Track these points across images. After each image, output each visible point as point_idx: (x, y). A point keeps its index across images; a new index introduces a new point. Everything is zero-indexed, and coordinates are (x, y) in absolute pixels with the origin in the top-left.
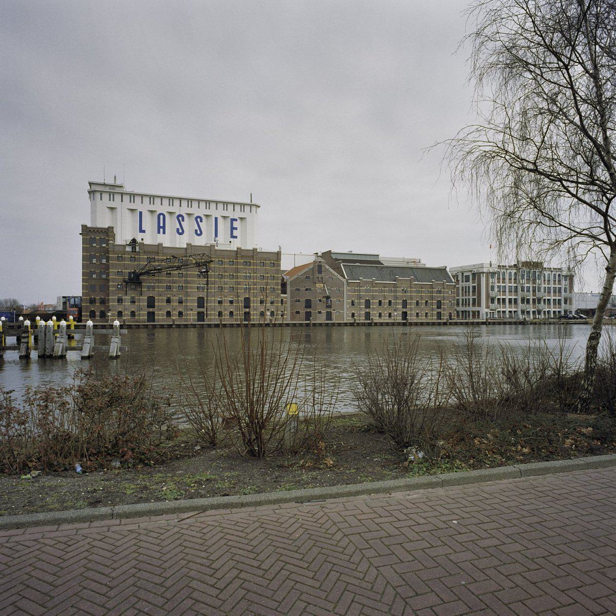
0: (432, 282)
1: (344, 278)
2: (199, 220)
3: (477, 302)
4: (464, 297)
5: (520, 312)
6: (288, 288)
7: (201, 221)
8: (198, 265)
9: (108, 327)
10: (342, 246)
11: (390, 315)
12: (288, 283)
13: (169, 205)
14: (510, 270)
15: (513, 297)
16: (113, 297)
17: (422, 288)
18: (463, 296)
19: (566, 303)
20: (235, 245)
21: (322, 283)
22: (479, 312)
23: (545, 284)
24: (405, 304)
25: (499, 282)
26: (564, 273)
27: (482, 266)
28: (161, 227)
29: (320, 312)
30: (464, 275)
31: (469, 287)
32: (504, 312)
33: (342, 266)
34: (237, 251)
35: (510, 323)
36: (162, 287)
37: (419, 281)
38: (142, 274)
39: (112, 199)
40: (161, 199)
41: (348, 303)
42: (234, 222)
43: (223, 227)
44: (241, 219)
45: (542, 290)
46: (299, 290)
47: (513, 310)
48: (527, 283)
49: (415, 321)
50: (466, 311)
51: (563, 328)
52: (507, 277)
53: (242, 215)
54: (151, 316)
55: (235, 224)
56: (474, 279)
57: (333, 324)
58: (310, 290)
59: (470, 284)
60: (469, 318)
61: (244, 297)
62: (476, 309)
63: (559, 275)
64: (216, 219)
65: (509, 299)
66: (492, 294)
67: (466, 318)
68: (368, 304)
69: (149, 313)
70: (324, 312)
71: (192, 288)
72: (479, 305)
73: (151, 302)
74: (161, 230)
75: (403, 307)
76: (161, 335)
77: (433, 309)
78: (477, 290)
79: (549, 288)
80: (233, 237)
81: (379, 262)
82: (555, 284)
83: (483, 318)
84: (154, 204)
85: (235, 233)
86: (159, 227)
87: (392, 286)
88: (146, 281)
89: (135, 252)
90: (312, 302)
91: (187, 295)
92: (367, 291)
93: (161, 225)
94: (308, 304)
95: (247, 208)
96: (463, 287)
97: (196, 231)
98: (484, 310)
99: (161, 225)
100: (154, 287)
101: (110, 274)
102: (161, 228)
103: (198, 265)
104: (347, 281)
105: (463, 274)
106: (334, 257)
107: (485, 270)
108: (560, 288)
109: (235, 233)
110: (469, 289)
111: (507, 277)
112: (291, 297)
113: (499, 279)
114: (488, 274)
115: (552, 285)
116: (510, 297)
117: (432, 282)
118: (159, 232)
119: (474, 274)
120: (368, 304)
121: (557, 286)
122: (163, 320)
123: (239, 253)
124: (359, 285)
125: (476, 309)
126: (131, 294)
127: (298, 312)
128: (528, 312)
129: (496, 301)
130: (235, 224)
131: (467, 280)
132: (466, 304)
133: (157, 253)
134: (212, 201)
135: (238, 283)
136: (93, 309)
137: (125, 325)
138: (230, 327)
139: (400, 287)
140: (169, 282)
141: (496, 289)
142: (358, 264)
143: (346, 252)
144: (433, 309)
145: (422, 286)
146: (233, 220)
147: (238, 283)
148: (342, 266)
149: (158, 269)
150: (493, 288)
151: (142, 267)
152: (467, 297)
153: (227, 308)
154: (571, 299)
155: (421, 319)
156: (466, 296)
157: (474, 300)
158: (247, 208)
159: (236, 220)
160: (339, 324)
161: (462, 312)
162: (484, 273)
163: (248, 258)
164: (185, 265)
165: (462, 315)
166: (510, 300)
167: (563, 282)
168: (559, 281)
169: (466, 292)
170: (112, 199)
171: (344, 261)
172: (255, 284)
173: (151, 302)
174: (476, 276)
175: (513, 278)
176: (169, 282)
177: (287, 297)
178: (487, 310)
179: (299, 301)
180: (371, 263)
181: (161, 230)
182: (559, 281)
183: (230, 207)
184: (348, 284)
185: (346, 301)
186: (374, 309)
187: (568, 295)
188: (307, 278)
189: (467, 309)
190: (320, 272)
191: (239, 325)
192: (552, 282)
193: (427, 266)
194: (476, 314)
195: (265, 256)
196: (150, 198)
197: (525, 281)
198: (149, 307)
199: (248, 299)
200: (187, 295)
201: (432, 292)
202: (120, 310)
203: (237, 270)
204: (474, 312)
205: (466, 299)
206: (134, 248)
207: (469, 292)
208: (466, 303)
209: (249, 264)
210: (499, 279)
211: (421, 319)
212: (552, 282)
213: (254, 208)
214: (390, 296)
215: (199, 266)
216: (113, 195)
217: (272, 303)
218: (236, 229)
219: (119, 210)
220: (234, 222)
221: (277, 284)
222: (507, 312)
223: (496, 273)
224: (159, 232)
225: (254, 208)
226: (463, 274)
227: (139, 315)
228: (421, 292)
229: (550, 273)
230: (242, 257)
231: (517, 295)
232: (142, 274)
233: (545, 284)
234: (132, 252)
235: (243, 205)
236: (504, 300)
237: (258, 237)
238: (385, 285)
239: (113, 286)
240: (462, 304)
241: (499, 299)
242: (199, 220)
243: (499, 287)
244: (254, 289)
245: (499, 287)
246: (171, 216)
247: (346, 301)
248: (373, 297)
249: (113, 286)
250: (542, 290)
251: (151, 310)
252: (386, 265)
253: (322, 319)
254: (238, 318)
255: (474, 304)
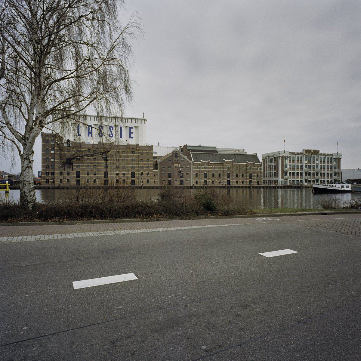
0: (246, 162)
1: (191, 160)
2: (111, 128)
3: (276, 175)
4: (270, 172)
5: (304, 181)
6: (159, 166)
7: (113, 129)
8: (102, 153)
9: (287, 187)
10: (193, 142)
11: (243, 182)
12: (158, 164)
13: (135, 123)
14: (298, 156)
15: (300, 172)
16: (57, 172)
17: (240, 166)
18: (269, 171)
19: (335, 175)
20: (133, 142)
21: (178, 164)
22: (277, 180)
23: (321, 163)
24: (229, 176)
25: (290, 162)
26: (334, 157)
27: (279, 153)
28: (90, 133)
29: (176, 180)
30: (270, 158)
31: (272, 165)
32: (293, 181)
33: (191, 154)
34: (127, 146)
35: (292, 188)
36: (84, 166)
37: (238, 162)
38: (73, 159)
39: (126, 122)
40: (131, 120)
41: (193, 175)
42: (131, 129)
43: (125, 133)
44: (136, 127)
45: (319, 167)
46: (164, 167)
47: (300, 179)
48: (309, 163)
49: (242, 186)
50: (270, 180)
51: (268, 190)
52: (296, 160)
53: (136, 125)
54: (78, 182)
55: (132, 130)
56: (275, 161)
57: (184, 187)
58: (170, 167)
59: (273, 164)
60: (272, 184)
61: (132, 171)
62: (276, 179)
63: (331, 158)
64: (121, 128)
65: (297, 173)
66: (285, 170)
67: (270, 184)
68: (206, 176)
69: (77, 180)
70: (179, 180)
71: (101, 166)
72: (278, 177)
73: (78, 174)
74: (90, 134)
75: (228, 178)
76: (233, 191)
77: (247, 179)
78: (276, 167)
79: (324, 166)
80: (130, 137)
81: (216, 151)
82: (328, 163)
83: (279, 184)
84: (137, 123)
85: (132, 135)
86: (89, 133)
87: (244, 165)
88: (75, 163)
89: (69, 147)
90: (172, 174)
91: (98, 170)
92: (204, 168)
93: (90, 132)
94: (170, 176)
95: (139, 121)
96: (269, 166)
97: (110, 134)
98: (280, 179)
99: (90, 132)
100: (79, 166)
101: (56, 159)
102: (101, 134)
103: (102, 153)
104: (193, 162)
105: (269, 158)
106: (188, 148)
107: (281, 155)
108: (302, 166)
109: (132, 135)
110: (272, 167)
111: (296, 160)
112: (160, 172)
113: (290, 161)
114: (283, 157)
115: (326, 165)
116: (298, 172)
117: (246, 162)
118: (89, 136)
119: (275, 158)
120: (206, 176)
121: (330, 165)
122: (44, 184)
123: (128, 147)
124: (200, 164)
125: (276, 179)
126: (67, 170)
127: (164, 180)
128: (310, 181)
129: (288, 174)
130: (132, 130)
131: (271, 162)
132: (270, 176)
133: (136, 149)
134: (133, 119)
135: (128, 164)
136: (47, 178)
137: (60, 187)
138: (187, 188)
139: (226, 166)
140: (88, 163)
141: (288, 167)
142: (201, 152)
143: (197, 145)
144: (247, 179)
145: (240, 165)
146: (131, 128)
147: (128, 164)
148: (191, 154)
149: (81, 156)
150: (286, 166)
151: (73, 155)
152: (271, 172)
153: (92, 177)
154: (339, 173)
155: (239, 185)
156: (271, 171)
157: (275, 173)
158: (139, 121)
159: (133, 128)
160: (188, 188)
161: (269, 180)
162: (280, 157)
163: (134, 149)
164: (94, 153)
165: (269, 183)
166: (298, 174)
167: (334, 162)
168: (331, 162)
169: (270, 169)
170: (126, 122)
171: (192, 150)
172: (137, 164)
173: (78, 174)
174: (276, 158)
175: (300, 160)
176: (88, 163)
177: (158, 171)
178: (282, 179)
179: (164, 174)
180: (211, 152)
181: (90, 134)
182: (331, 162)
183: (129, 121)
184: (193, 164)
185: (192, 174)
186: (209, 179)
187: (337, 170)
188: (169, 160)
189: (271, 179)
190: (176, 157)
191: (224, 187)
192: (296, 161)
193: (248, 153)
194: (276, 182)
195: (144, 148)
196: (135, 120)
197: (307, 162)
198: (77, 177)
199: (134, 173)
200: (98, 170)
201: (246, 169)
202: (61, 179)
203: (127, 157)
204: (275, 180)
205: (269, 173)
206: (69, 145)
207: (272, 168)
208: (271, 176)
209: (134, 153)
210: (290, 161)
211: (239, 185)
212: (296, 161)
213: (143, 121)
214: (219, 171)
215: (102, 154)
216: (137, 120)
217: (148, 175)
218: (133, 133)
219: (139, 128)
220: (131, 129)
221: (151, 164)
222: (296, 181)
223: (288, 157)
224: (89, 136)
225: (143, 121)
226: (269, 158)
227: (91, 182)
228: (240, 169)
229: (294, 156)
230: (130, 149)
231: (302, 171)
232: (73, 159)
233: (321, 163)
234: (68, 147)
235: (136, 120)
236: (293, 173)
237: (145, 137)
238: (216, 165)
239: (57, 165)
240: (269, 176)
241: (321, 173)
242: (111, 128)
243: (290, 165)
244: (137, 167)
245: (290, 165)
246: (136, 129)
247: (192, 174)
248: (209, 172)
249: (57, 165)
250: (319, 167)
251: (133, 179)
252: (220, 152)
253: (177, 184)
254: (225, 184)
255: (275, 176)
